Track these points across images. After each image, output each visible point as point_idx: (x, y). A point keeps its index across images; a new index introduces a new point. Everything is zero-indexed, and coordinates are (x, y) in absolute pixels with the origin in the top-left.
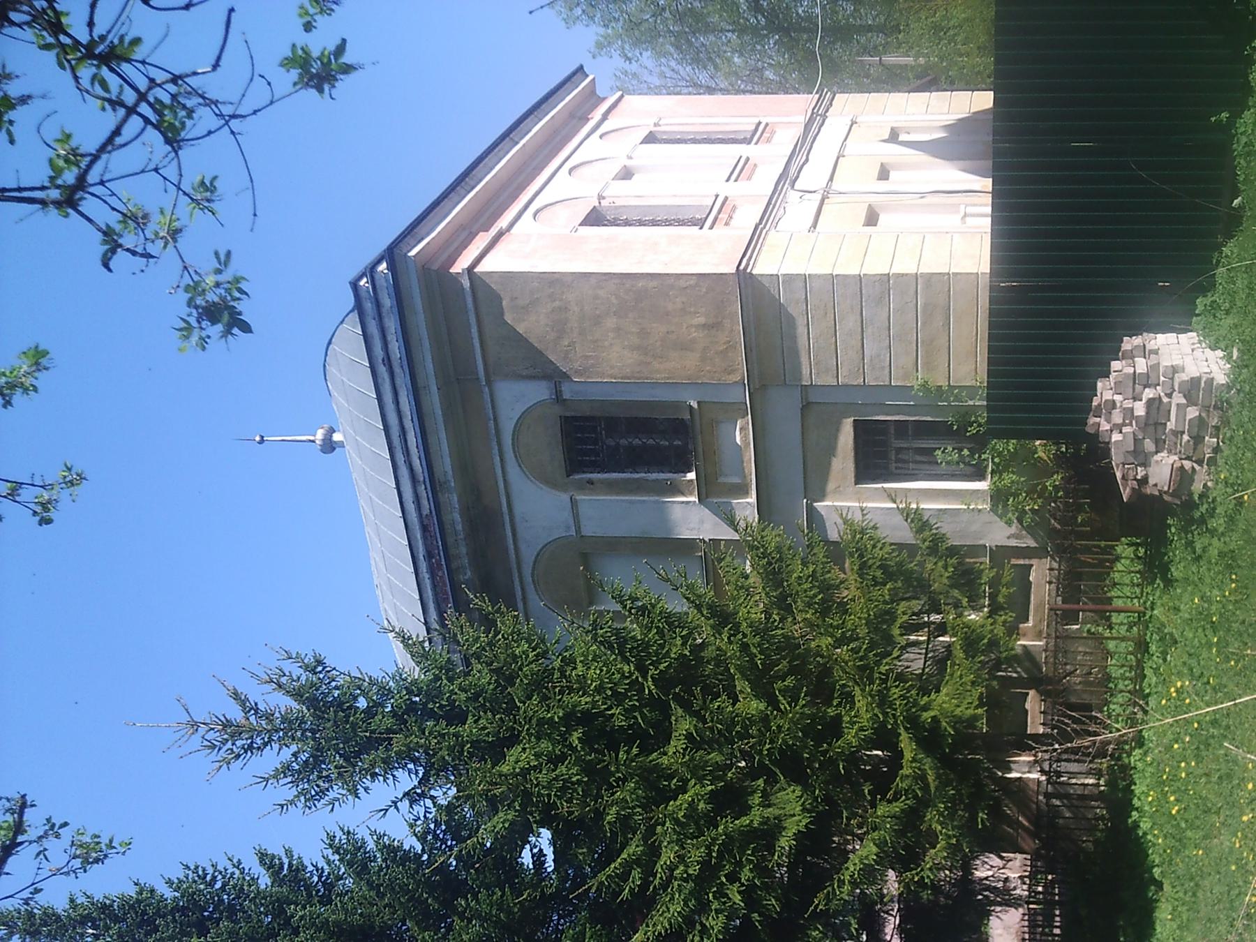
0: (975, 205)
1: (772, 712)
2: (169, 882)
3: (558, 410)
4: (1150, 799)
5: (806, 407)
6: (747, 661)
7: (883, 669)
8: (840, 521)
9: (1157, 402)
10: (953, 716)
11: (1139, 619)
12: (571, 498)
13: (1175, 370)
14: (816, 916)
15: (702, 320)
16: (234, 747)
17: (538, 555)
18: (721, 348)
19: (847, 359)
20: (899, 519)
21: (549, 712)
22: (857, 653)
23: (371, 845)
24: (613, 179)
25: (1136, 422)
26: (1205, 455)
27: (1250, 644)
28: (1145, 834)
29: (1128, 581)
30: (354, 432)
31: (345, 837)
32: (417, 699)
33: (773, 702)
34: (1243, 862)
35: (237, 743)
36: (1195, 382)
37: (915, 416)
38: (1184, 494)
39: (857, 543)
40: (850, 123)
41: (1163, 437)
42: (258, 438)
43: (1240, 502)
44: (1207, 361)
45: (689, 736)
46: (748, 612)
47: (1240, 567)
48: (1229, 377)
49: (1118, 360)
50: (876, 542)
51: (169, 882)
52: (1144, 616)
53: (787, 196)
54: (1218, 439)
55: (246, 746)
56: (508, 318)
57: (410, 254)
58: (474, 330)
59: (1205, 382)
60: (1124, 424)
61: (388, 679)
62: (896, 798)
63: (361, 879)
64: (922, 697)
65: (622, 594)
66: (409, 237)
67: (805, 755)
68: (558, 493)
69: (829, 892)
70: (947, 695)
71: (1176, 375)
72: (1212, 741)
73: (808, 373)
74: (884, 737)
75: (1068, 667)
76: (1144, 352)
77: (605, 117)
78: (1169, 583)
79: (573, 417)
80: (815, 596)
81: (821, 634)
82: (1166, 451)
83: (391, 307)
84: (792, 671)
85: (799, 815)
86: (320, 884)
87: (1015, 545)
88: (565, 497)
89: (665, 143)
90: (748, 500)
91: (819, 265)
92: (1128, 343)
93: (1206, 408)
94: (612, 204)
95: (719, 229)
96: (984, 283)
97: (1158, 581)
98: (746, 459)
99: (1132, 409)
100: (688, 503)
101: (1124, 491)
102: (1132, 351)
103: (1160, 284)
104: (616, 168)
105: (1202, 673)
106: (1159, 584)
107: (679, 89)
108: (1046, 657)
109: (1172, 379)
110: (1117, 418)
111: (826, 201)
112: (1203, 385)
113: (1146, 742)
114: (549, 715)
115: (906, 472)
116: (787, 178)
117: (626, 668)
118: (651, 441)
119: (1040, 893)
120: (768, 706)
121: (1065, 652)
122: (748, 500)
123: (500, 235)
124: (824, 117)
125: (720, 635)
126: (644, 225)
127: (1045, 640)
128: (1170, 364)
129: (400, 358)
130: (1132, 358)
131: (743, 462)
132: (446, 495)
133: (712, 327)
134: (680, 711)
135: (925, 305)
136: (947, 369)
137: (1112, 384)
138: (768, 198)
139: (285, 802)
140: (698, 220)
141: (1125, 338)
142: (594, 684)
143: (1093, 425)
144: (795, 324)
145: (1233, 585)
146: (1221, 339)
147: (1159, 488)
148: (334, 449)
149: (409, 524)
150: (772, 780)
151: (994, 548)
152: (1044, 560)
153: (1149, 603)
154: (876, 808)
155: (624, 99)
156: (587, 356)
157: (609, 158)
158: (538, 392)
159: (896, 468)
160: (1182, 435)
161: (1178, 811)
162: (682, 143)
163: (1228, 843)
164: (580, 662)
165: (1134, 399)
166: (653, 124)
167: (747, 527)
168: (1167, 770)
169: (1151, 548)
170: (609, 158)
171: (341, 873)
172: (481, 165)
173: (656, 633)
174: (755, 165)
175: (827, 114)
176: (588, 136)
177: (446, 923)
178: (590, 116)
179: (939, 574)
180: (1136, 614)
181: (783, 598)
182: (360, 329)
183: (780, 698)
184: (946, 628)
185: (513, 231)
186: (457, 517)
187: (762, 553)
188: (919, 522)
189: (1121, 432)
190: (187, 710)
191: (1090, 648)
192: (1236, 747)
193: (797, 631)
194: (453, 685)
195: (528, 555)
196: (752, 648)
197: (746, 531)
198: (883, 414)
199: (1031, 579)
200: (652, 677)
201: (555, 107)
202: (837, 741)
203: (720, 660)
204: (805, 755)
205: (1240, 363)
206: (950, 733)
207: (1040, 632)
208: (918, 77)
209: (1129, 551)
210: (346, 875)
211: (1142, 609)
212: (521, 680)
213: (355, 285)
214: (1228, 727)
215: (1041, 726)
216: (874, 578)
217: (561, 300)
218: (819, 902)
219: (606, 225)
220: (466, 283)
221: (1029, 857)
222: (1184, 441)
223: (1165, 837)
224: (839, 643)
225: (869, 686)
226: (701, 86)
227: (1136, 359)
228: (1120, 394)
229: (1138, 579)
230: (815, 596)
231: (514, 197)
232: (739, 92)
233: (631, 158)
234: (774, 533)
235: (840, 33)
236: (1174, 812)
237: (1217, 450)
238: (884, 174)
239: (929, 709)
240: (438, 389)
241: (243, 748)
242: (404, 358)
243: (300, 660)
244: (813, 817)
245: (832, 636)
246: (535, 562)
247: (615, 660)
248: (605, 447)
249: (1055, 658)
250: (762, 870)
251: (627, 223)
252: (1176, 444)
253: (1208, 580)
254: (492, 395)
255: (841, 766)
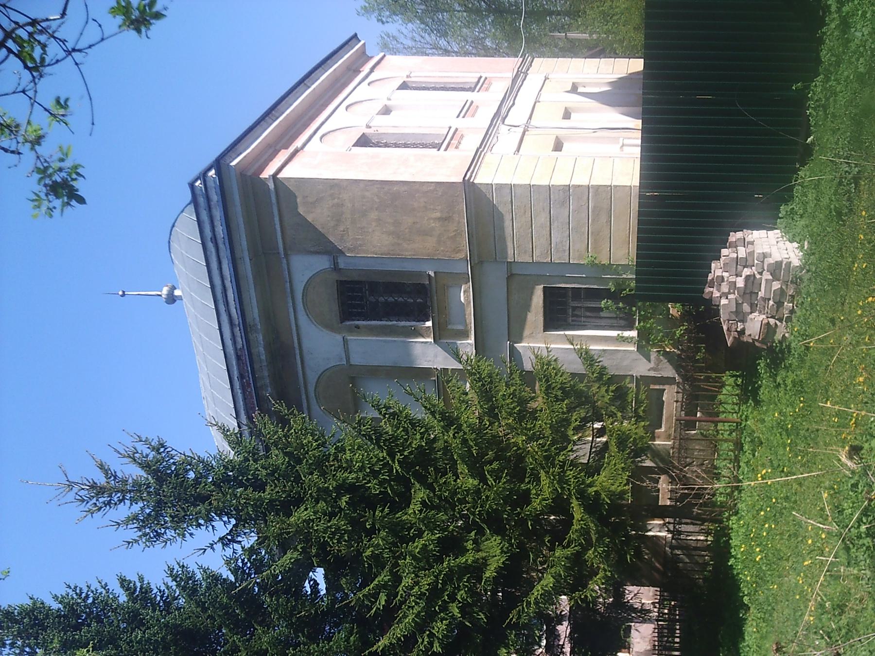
0: (629, 138)
1: (482, 487)
2: (56, 597)
3: (335, 277)
4: (742, 550)
5: (510, 277)
6: (466, 451)
7: (561, 458)
8: (533, 357)
9: (752, 278)
10: (609, 491)
11: (737, 427)
12: (343, 338)
13: (765, 255)
14: (511, 626)
15: (438, 215)
16: (97, 502)
17: (319, 377)
18: (452, 234)
19: (540, 243)
20: (574, 357)
21: (325, 483)
22: (543, 447)
23: (199, 576)
24: (377, 114)
25: (738, 291)
26: (784, 315)
27: (811, 445)
28: (738, 574)
29: (730, 402)
30: (189, 288)
31: (181, 569)
32: (231, 473)
33: (484, 480)
34: (805, 593)
35: (100, 499)
36: (779, 264)
37: (586, 284)
38: (769, 342)
39: (545, 372)
40: (544, 79)
41: (756, 302)
42: (121, 293)
43: (807, 348)
44: (787, 250)
45: (423, 503)
46: (468, 417)
47: (806, 392)
48: (801, 261)
49: (726, 248)
50: (557, 371)
51: (56, 597)
52: (741, 425)
53: (499, 129)
54: (793, 304)
55: (106, 502)
56: (301, 210)
57: (231, 164)
58: (277, 219)
59: (785, 265)
60: (729, 293)
61: (211, 459)
62: (568, 546)
63: (192, 599)
64: (588, 478)
65: (379, 404)
66: (231, 152)
67: (505, 516)
68: (334, 334)
69: (520, 610)
70: (605, 477)
71: (766, 259)
72: (784, 511)
73: (512, 253)
74: (560, 505)
75: (688, 460)
76: (744, 242)
77: (372, 70)
78: (758, 403)
79: (345, 281)
80: (514, 408)
81: (518, 434)
82: (757, 312)
83: (217, 201)
84: (496, 458)
85: (499, 556)
86: (161, 601)
87: (653, 375)
88: (339, 338)
89: (414, 89)
90: (468, 341)
91: (521, 179)
92: (734, 237)
93: (786, 282)
94: (376, 132)
95: (451, 151)
96: (635, 192)
97: (750, 401)
98: (467, 313)
99: (735, 283)
100: (426, 342)
101: (729, 339)
102: (736, 242)
103: (756, 196)
104: (379, 107)
105: (779, 465)
106: (751, 404)
107: (424, 50)
108: (673, 453)
109: (763, 262)
110: (725, 288)
111: (526, 132)
112: (784, 266)
113: (740, 512)
114: (326, 485)
115: (580, 323)
116: (499, 116)
117: (381, 455)
118: (401, 299)
119: (666, 614)
120: (480, 483)
121: (686, 449)
122: (468, 341)
123: (297, 151)
124: (526, 74)
125: (447, 432)
126: (398, 147)
127: (672, 441)
128: (761, 252)
129: (223, 238)
130: (736, 247)
131: (465, 315)
132: (255, 335)
133: (445, 219)
134: (418, 485)
135: (595, 207)
136: (609, 253)
137: (722, 265)
138: (486, 130)
139: (131, 540)
140: (437, 144)
141: (731, 233)
142: (358, 464)
143: (708, 293)
144: (503, 219)
145: (802, 405)
146: (797, 235)
147: (752, 337)
148: (175, 301)
149: (228, 355)
150: (481, 532)
151: (639, 377)
152: (673, 386)
153: (744, 416)
154: (554, 551)
155: (385, 58)
156: (357, 238)
157: (374, 99)
158: (322, 263)
159: (572, 321)
160: (768, 301)
161: (761, 559)
162: (425, 90)
163: (794, 581)
164: (349, 450)
165: (737, 275)
166: (406, 76)
167: (468, 359)
168: (754, 530)
169: (746, 379)
170: (374, 99)
171: (176, 595)
172: (284, 102)
173: (403, 430)
174: (477, 107)
175: (528, 72)
176: (360, 83)
177: (250, 631)
178: (361, 70)
179: (603, 396)
180: (735, 424)
181: (492, 409)
182: (195, 216)
183: (488, 476)
184: (605, 431)
185: (306, 149)
186: (262, 349)
187: (478, 378)
188: (588, 357)
189: (727, 298)
190: (65, 474)
191: (703, 447)
192: (801, 515)
193: (501, 432)
194: (257, 464)
195: (312, 378)
196: (470, 441)
197: (467, 362)
198: (564, 283)
199: (664, 399)
200: (398, 461)
201: (337, 62)
202: (527, 507)
203: (447, 450)
204: (505, 516)
205: (810, 252)
206: (607, 502)
207: (670, 435)
208: (590, 49)
209: (731, 381)
210: (180, 597)
211: (739, 420)
212: (307, 461)
213: (192, 186)
214: (795, 502)
215: (668, 500)
216: (556, 396)
217: (339, 198)
218: (513, 615)
219: (371, 146)
220: (271, 185)
221: (659, 589)
222: (770, 305)
223: (752, 576)
224: (530, 439)
225: (552, 468)
226: (441, 49)
227: (738, 248)
228: (727, 272)
229: (737, 400)
230: (514, 408)
231: (306, 126)
232: (467, 54)
233: (390, 100)
234: (486, 364)
235: (537, 15)
236: (757, 559)
237: (792, 311)
238: (567, 115)
239: (593, 486)
240: (250, 260)
241: (104, 503)
242: (226, 237)
243: (148, 443)
244: (508, 556)
245: (526, 435)
246: (317, 383)
247: (374, 448)
248: (368, 302)
249: (679, 453)
250: (472, 592)
251: (386, 145)
252: (764, 307)
253: (784, 401)
254: (288, 264)
255: (529, 524)
